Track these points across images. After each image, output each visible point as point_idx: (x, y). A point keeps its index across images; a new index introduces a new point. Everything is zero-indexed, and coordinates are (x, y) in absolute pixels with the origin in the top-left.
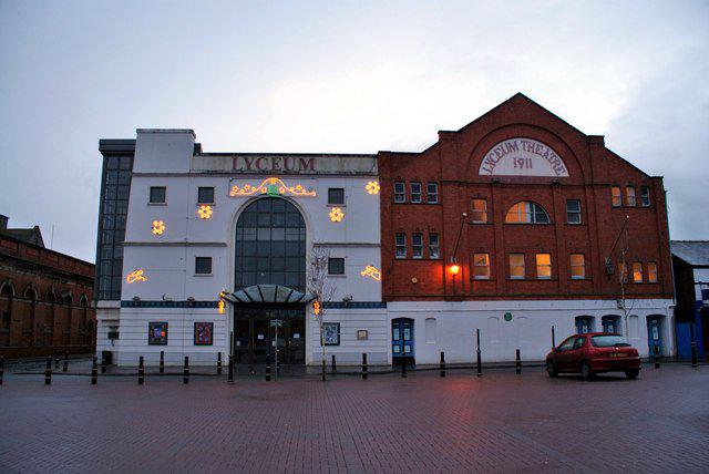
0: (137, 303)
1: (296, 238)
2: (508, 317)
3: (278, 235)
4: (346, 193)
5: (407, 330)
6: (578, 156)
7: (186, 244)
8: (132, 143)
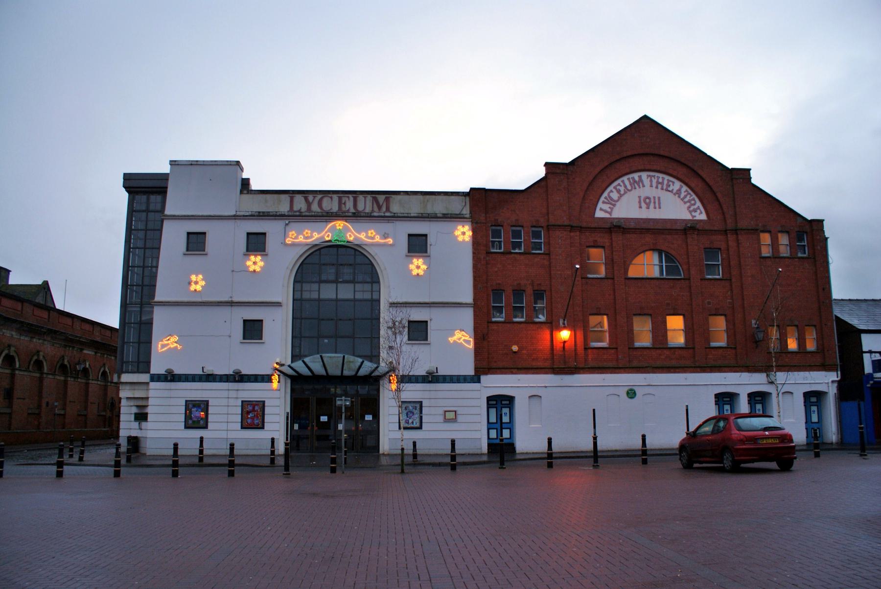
0: (171, 377)
1: (367, 296)
2: (631, 394)
5: (506, 410)
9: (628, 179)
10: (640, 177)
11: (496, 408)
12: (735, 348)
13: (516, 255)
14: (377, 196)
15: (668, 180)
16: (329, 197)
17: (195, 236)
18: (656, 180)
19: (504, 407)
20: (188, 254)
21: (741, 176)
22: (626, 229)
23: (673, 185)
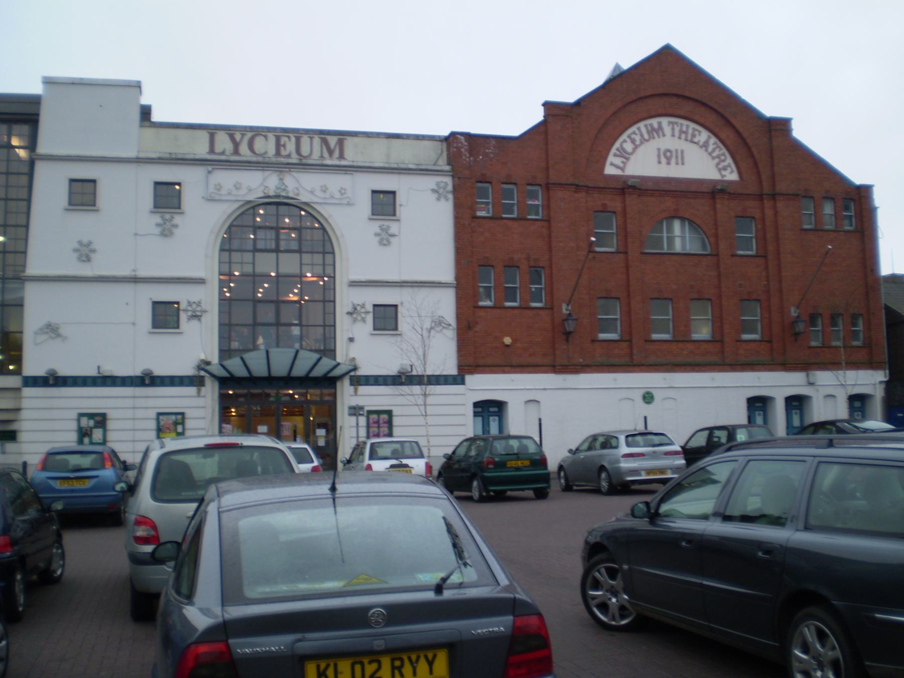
0: (53, 380)
4: (400, 199)
6: (754, 149)
7: (135, 280)
8: (34, 101)
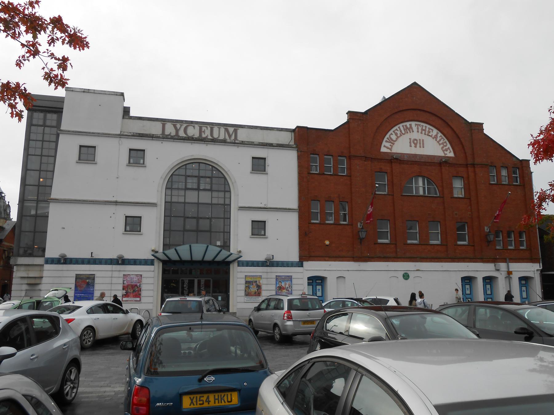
0: (64, 260)
1: (221, 201)
2: (406, 276)
3: (205, 198)
5: (319, 287)
9: (403, 126)
10: (410, 125)
11: (312, 285)
12: (473, 246)
13: (328, 176)
14: (228, 128)
15: (429, 128)
16: (193, 126)
17: (86, 149)
18: (421, 128)
19: (487, 284)
20: (80, 163)
21: (478, 128)
22: (402, 161)
23: (432, 132)
